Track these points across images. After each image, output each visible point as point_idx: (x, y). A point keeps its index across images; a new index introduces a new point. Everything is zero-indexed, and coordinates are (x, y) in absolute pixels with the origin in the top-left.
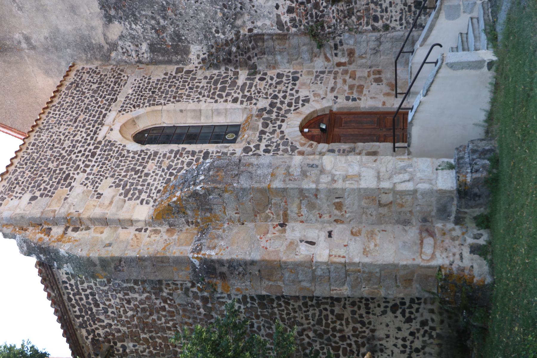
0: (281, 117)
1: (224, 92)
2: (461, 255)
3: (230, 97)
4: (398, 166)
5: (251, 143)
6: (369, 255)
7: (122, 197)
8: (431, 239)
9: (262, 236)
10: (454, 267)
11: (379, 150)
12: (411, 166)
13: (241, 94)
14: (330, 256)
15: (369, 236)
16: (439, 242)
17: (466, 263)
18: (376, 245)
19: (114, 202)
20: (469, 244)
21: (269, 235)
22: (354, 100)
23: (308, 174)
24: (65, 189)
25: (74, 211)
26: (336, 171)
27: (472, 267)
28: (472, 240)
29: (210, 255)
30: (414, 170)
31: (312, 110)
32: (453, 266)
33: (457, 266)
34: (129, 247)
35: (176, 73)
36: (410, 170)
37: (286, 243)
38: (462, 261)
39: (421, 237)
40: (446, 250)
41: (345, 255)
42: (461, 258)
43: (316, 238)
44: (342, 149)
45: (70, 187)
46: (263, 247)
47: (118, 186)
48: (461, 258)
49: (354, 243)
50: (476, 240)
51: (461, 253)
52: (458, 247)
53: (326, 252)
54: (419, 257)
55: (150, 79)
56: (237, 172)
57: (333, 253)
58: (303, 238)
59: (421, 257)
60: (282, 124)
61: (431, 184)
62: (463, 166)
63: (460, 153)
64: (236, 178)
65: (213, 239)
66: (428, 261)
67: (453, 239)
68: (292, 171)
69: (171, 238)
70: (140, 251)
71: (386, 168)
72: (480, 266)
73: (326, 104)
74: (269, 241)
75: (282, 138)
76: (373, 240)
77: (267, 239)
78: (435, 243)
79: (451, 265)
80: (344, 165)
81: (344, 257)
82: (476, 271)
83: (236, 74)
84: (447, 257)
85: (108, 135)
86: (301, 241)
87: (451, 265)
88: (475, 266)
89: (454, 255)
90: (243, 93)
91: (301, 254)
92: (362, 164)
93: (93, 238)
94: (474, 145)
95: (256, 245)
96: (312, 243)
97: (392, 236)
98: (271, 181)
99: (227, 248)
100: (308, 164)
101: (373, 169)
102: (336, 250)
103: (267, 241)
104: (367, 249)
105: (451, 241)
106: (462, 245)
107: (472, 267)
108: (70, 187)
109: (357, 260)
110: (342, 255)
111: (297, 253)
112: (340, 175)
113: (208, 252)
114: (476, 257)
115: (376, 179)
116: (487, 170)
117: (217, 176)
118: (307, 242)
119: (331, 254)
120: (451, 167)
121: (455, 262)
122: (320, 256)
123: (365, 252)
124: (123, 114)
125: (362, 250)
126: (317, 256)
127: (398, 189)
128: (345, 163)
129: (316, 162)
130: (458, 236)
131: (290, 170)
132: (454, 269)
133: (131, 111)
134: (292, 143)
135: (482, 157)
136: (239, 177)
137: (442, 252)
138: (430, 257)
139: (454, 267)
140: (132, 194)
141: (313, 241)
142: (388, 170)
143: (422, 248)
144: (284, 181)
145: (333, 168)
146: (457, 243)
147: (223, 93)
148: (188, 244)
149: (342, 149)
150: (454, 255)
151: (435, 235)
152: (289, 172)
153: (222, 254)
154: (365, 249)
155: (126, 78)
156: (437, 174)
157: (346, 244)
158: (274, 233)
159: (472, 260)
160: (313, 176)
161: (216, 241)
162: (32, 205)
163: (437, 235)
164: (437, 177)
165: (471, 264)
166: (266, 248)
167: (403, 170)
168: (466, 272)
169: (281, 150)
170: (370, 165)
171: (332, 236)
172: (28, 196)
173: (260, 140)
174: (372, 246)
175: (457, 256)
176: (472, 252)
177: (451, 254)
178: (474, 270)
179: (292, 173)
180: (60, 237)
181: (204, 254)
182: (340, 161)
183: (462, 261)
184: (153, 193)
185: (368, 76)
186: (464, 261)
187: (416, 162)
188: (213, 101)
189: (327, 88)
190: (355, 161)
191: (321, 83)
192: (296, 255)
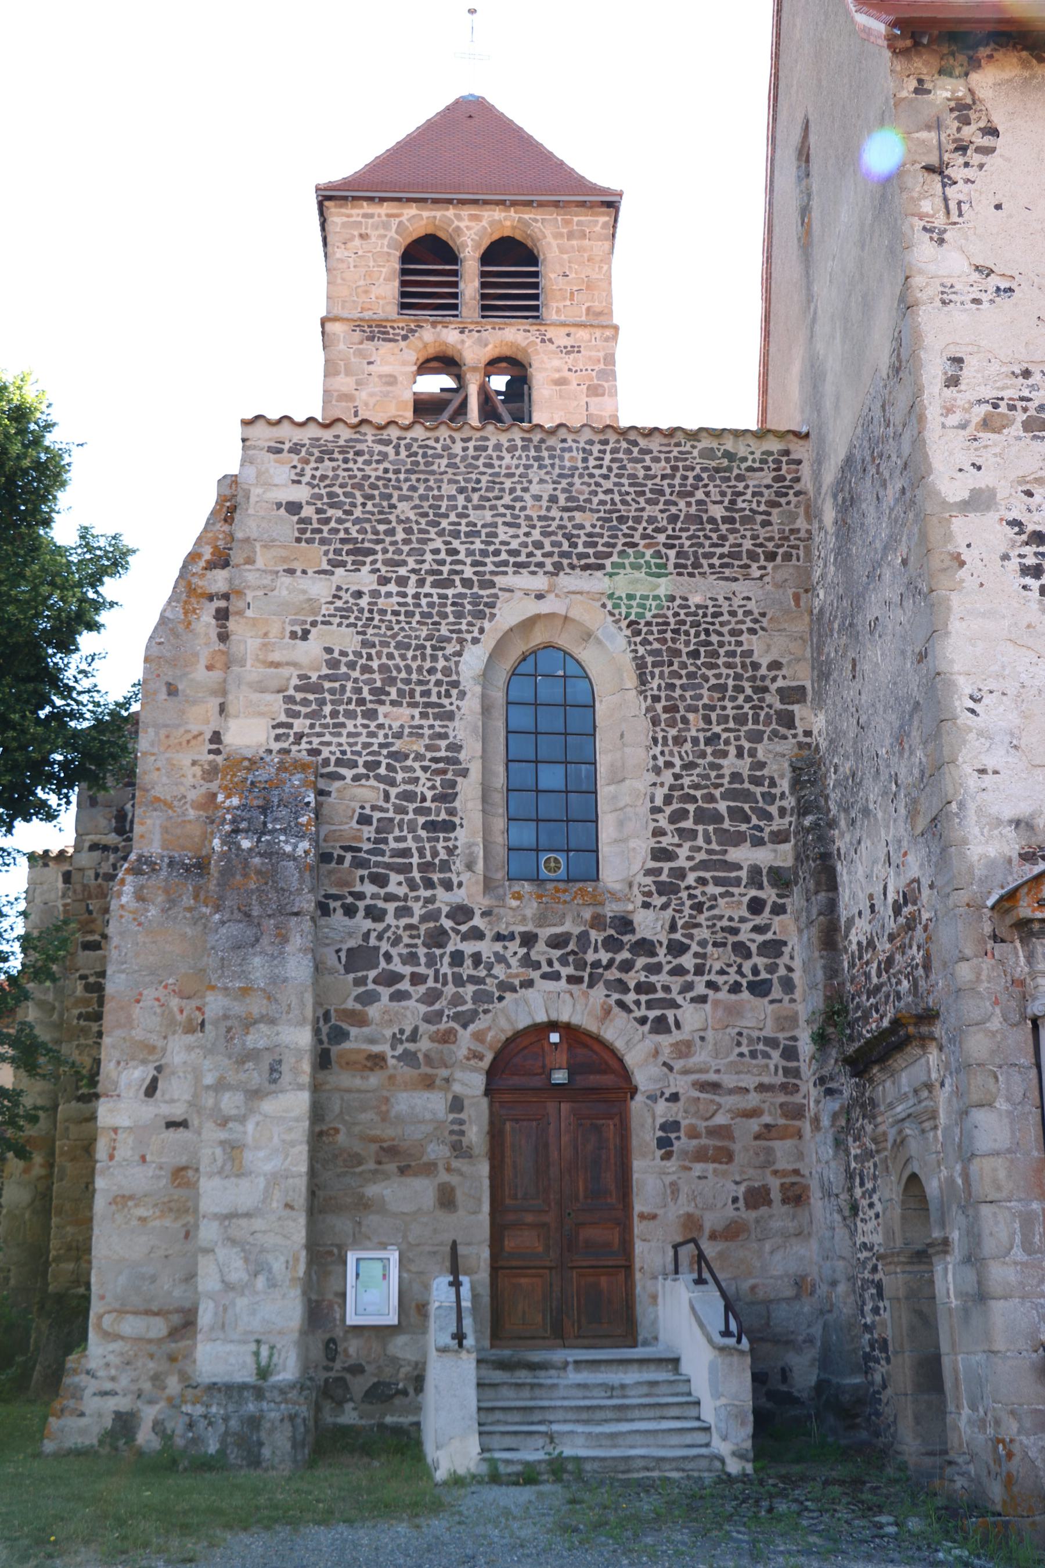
0: (591, 975)
1: (696, 823)
2: (113, 1393)
3: (676, 840)
4: (270, 1258)
5: (486, 919)
6: (114, 1207)
7: (295, 681)
8: (164, 1332)
9: (171, 987)
10: (82, 1379)
11: (461, 1212)
12: (272, 1284)
13: (688, 864)
14: (115, 1130)
15: (173, 1204)
16: (153, 1348)
17: (91, 1404)
18: (143, 1220)
19: (280, 670)
20: (139, 1411)
21: (175, 1002)
22: (664, 1143)
23: (250, 1065)
24: (324, 559)
25: (249, 599)
26: (257, 1124)
27: (82, 1414)
28: (152, 1418)
29: (120, 894)
30: (257, 1293)
31: (619, 1045)
32: (83, 1377)
33: (82, 1384)
34: (163, 732)
35: (780, 690)
36: (260, 1282)
37: (154, 1039)
38: (95, 1394)
39: (169, 1312)
40: (128, 1364)
41: (117, 1158)
42: (105, 1394)
43: (167, 1097)
44: (463, 1128)
45: (329, 568)
46: (141, 994)
47: (333, 664)
48: (105, 1394)
49: (150, 1174)
50: (151, 1424)
51: (116, 1394)
52: (134, 1387)
53: (123, 1120)
54: (109, 1308)
55: (752, 631)
56: (255, 913)
57: (121, 1136)
58: (167, 1071)
59: (109, 1312)
60: (564, 980)
61: (212, 1329)
62: (230, 1398)
63: (276, 1393)
64: (238, 916)
65: (166, 891)
66: (99, 1326)
67: (157, 1379)
68: (258, 1030)
69: (188, 806)
70: (153, 754)
71: (265, 1232)
72: (83, 1432)
73: (644, 1077)
74: (156, 1003)
75: (506, 987)
76: (158, 1214)
77: (163, 1000)
78: (150, 1341)
79: (88, 1372)
80: (276, 1140)
81: (111, 1157)
82: (71, 1422)
83: (779, 838)
84: (107, 1365)
85: (519, 594)
86: (159, 1069)
87: (88, 1372)
88: (83, 1422)
89: (113, 1379)
90: (692, 869)
91: (120, 1073)
92: (275, 1179)
93: (196, 655)
94: (277, 1423)
95: (147, 979)
96: (151, 1090)
97: (170, 1252)
98: (226, 989)
99: (140, 924)
100: (280, 1062)
101: (264, 1201)
102: (130, 1141)
103: (158, 1000)
104: (130, 1203)
105: (152, 1373)
106: (139, 1396)
107: (82, 1414)
108: (329, 568)
109: (100, 1183)
110: (116, 1153)
111: (122, 1064)
112: (245, 1133)
113: (128, 889)
114: (108, 1423)
115: (225, 1211)
116: (186, 1447)
117: (245, 875)
118: (154, 1081)
119: (120, 1131)
120: (263, 1373)
121: (93, 1381)
122: (111, 1111)
123: (121, 1200)
124: (604, 606)
125: (127, 1193)
126: (111, 1105)
127: (199, 1258)
128: (284, 1141)
129: (286, 1078)
130: (164, 1388)
131: (262, 1026)
132: (76, 1379)
133: (617, 622)
134: (486, 1012)
135: (229, 1440)
136: (240, 921)
137: (122, 1354)
138: (110, 1330)
139: (82, 1379)
140: (305, 699)
141: (158, 1093)
142: (258, 1235)
143: (136, 1313)
144: (226, 1017)
145: (266, 1116)
146: (147, 1386)
147: (691, 820)
148: (164, 847)
149: (463, 1128)
150: (113, 1379)
151: (176, 1342)
152: (255, 1022)
153: (121, 917)
154: (131, 1197)
155: (757, 574)
156: (245, 1342)
157: (148, 1158)
158: (181, 1011)
159: (100, 1415)
160: (243, 1076)
161: (160, 899)
162: (275, 513)
163: (173, 1345)
164: (232, 1341)
165: (87, 1412)
166: (138, 1001)
167: (258, 1268)
168: (72, 1403)
169: (461, 990)
170: (277, 1194)
171: (172, 1130)
172: (301, 494)
173: (499, 937)
174: (141, 1212)
175: (108, 1386)
176: (119, 1416)
177: (113, 1372)
178: (75, 1419)
179: (252, 1030)
180: (199, 591)
181: (123, 882)
182: (290, 1129)
183: (95, 1394)
184: (310, 743)
185: (775, 1173)
186: (97, 1399)
187: (284, 1296)
188: (659, 802)
189: (718, 1071)
190: (287, 1162)
191: (741, 1055)
192: (118, 1063)
